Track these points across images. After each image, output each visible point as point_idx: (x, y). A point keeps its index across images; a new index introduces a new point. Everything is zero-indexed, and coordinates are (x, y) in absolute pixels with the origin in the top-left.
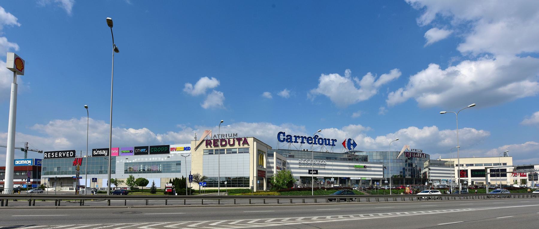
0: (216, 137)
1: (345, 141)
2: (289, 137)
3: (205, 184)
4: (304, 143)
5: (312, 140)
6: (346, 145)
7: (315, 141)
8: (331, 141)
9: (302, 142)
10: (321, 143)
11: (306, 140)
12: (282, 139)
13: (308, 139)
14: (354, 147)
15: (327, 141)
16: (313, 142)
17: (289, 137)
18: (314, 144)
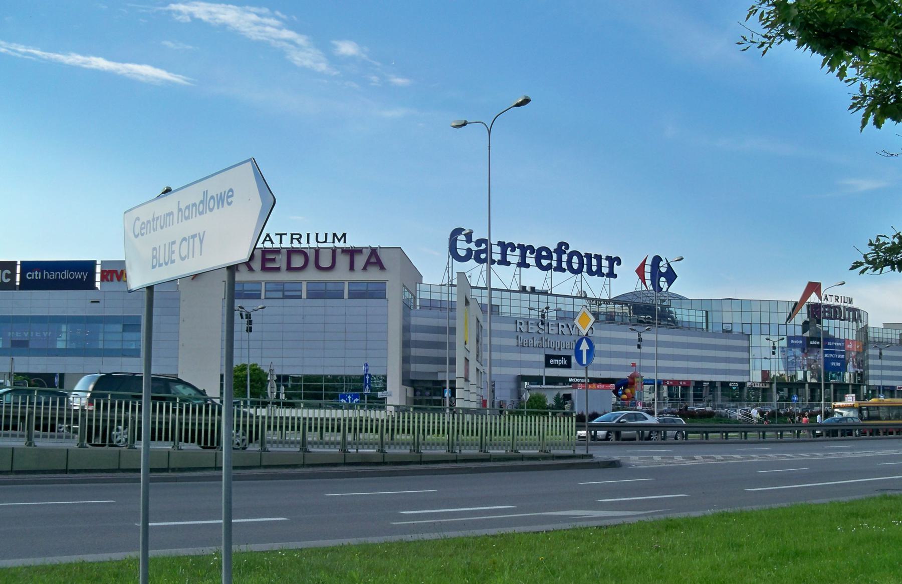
0: (271, 240)
1: (644, 264)
2: (483, 246)
3: (357, 400)
4: (528, 266)
5: (549, 257)
6: (648, 276)
7: (560, 261)
8: (605, 263)
9: (523, 264)
10: (575, 266)
11: (533, 256)
12: (462, 253)
13: (541, 254)
14: (670, 281)
15: (594, 262)
16: (554, 264)
17: (483, 246)
18: (556, 269)
